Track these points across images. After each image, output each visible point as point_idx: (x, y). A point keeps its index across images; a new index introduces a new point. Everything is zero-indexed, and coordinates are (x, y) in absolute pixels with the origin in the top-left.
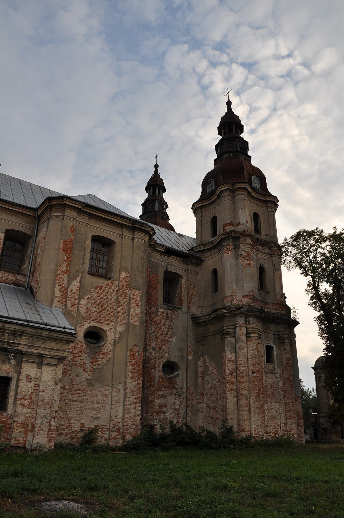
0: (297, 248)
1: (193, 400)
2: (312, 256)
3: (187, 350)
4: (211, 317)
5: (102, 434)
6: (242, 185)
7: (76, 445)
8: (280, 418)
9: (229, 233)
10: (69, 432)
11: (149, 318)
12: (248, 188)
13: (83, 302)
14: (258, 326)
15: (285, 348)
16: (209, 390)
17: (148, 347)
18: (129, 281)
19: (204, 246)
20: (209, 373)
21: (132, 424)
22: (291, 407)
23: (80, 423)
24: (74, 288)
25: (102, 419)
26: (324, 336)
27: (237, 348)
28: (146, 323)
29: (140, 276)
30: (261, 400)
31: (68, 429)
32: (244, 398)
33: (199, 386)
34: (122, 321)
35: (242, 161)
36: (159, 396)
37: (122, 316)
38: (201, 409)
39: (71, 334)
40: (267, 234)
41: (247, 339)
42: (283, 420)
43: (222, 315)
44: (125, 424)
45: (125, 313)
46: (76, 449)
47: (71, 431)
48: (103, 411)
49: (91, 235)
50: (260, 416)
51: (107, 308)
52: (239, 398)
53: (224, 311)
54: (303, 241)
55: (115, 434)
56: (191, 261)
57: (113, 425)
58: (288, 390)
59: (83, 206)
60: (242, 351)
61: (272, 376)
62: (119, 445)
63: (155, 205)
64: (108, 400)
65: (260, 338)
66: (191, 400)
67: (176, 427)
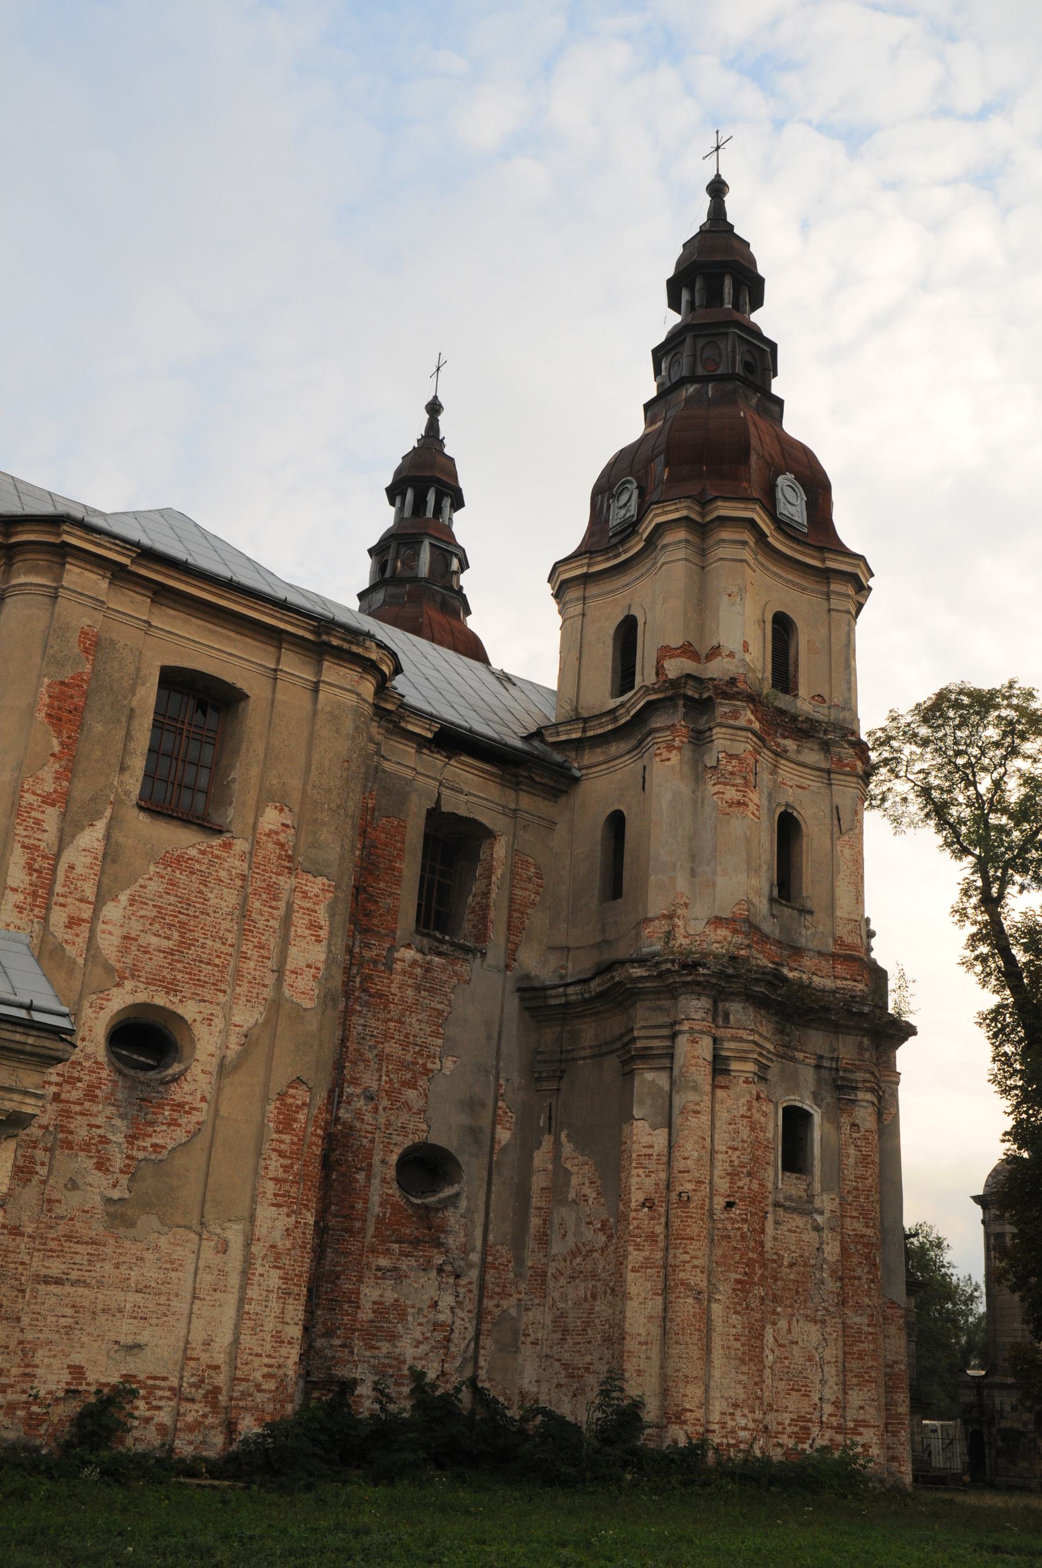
0: (936, 750)
1: (504, 1295)
2: (985, 784)
3: (496, 1107)
4: (590, 992)
5: (149, 1409)
6: (735, 509)
7: (44, 1452)
8: (823, 1382)
9: (674, 684)
10: (24, 1397)
11: (361, 983)
12: (758, 520)
13: (112, 911)
14: (761, 1035)
15: (857, 1121)
16: (565, 1261)
17: (348, 1090)
18: (291, 844)
19: (581, 726)
20: (572, 1195)
21: (267, 1376)
22: (863, 1342)
23: (69, 1367)
24: (83, 859)
25: (154, 1353)
26: (1008, 1083)
27: (676, 1111)
28: (348, 998)
29: (333, 829)
30: (752, 1309)
31: (18, 1388)
32: (688, 1297)
33: (532, 1244)
34: (256, 991)
35: (748, 417)
36: (379, 1274)
37: (255, 969)
38: (531, 1331)
39: (55, 1031)
40: (819, 695)
41: (713, 1079)
42: (831, 1388)
43: (629, 986)
44: (239, 1374)
45: (269, 958)
46: (42, 1468)
47: (30, 1396)
48: (161, 1321)
49: (159, 664)
50: (744, 1369)
51: (201, 940)
52: (672, 1297)
53: (638, 972)
54: (958, 727)
55: (197, 1411)
56: (533, 779)
57: (193, 1375)
58: (855, 1278)
59: (134, 555)
60: (693, 1121)
61: (800, 1221)
62: (210, 1454)
63: (419, 555)
64: (182, 1282)
65: (763, 1079)
66: (499, 1294)
67: (433, 1391)
